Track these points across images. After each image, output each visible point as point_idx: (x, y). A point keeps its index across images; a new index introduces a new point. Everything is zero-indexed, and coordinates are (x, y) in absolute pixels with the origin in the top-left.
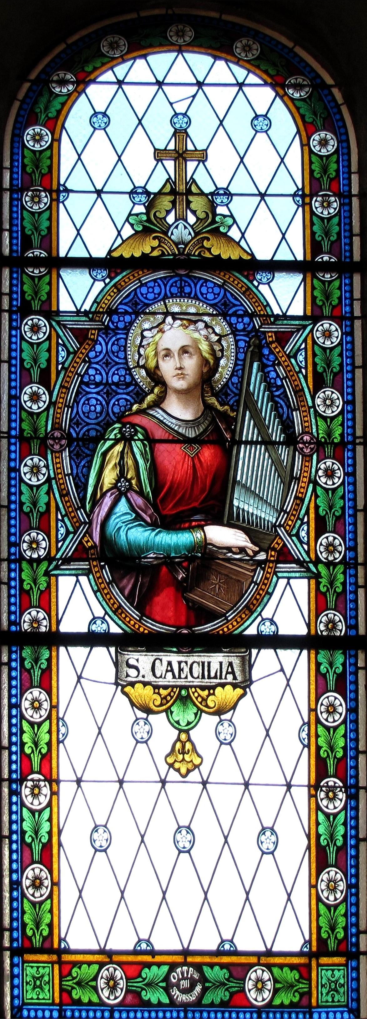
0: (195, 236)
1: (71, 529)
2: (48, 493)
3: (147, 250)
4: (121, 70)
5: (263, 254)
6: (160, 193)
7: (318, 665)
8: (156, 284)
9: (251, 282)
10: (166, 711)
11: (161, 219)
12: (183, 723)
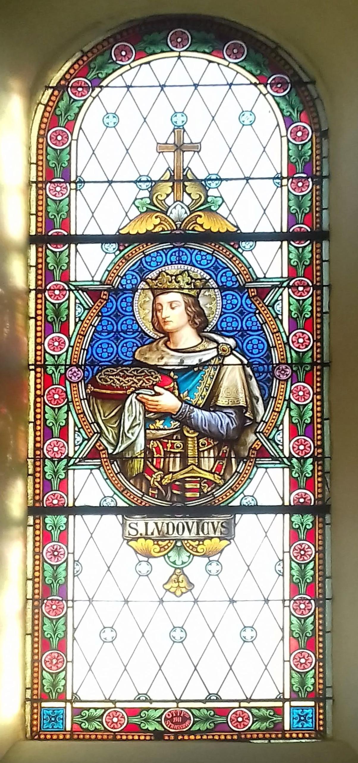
0: (191, 214)
1: (86, 437)
3: (150, 228)
4: (129, 77)
5: (246, 228)
7: (291, 522)
8: (159, 254)
9: (237, 249)
10: (164, 556)
11: (161, 201)
12: (179, 562)
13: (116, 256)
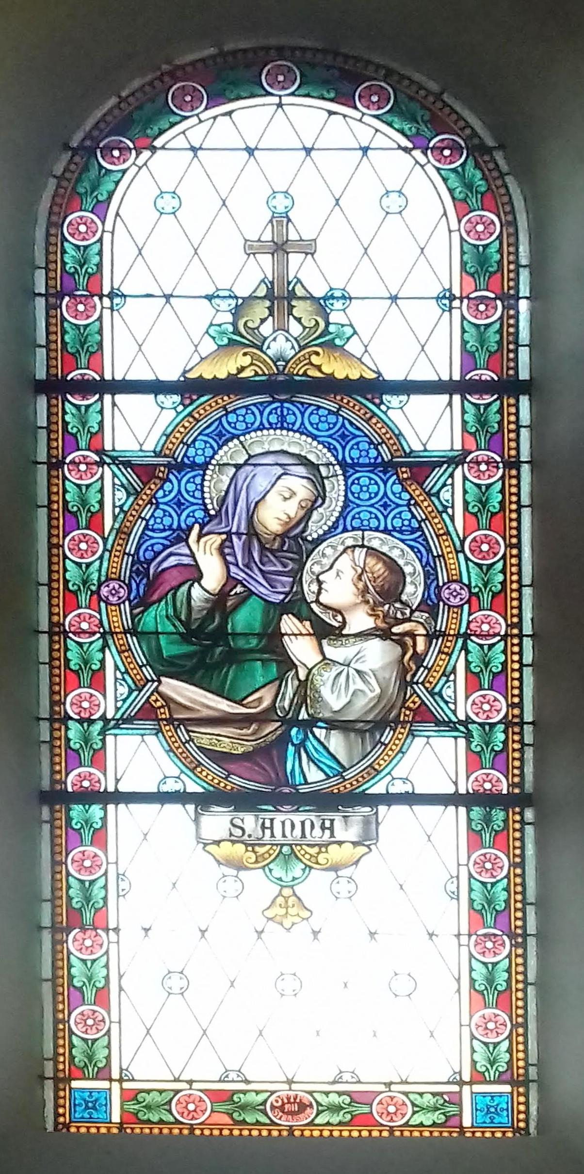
0: (299, 351)
2: (102, 650)
4: (196, 136)
6: (252, 298)
8: (249, 412)
9: (378, 406)
10: (263, 868)
11: (253, 329)
13: (178, 413)
